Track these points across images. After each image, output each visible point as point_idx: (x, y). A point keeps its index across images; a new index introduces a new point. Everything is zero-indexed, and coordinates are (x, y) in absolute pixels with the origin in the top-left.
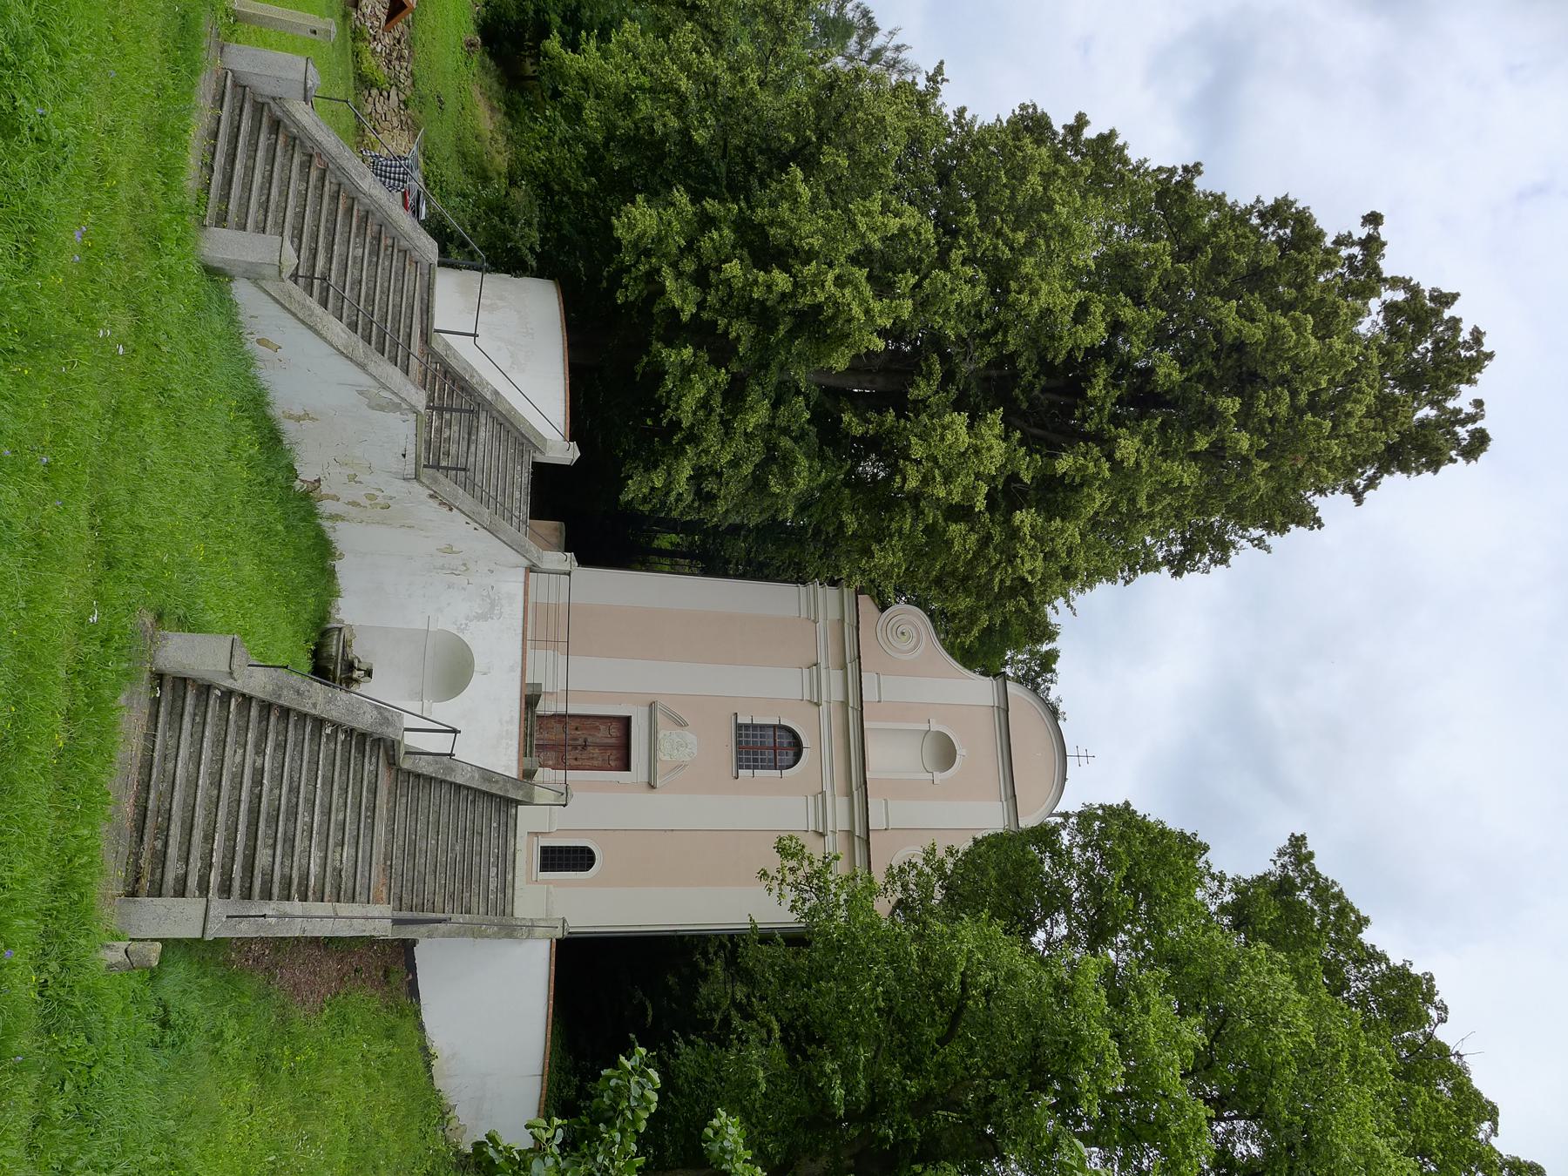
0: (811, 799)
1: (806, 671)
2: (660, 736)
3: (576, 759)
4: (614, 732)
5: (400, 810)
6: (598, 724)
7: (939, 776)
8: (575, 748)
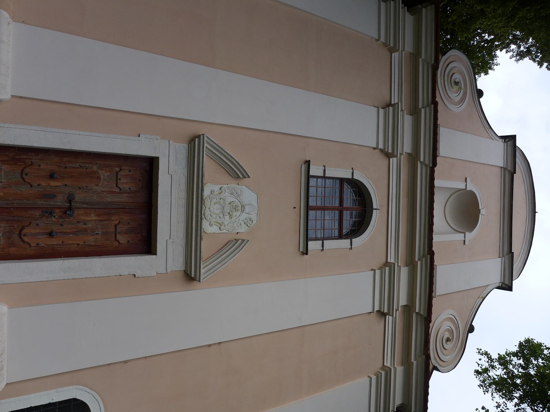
0: (378, 272)
1: (382, 111)
2: (206, 193)
3: (51, 234)
4: (126, 184)
5: (403, 11)
6: (95, 168)
7: (470, 236)
8: (49, 212)
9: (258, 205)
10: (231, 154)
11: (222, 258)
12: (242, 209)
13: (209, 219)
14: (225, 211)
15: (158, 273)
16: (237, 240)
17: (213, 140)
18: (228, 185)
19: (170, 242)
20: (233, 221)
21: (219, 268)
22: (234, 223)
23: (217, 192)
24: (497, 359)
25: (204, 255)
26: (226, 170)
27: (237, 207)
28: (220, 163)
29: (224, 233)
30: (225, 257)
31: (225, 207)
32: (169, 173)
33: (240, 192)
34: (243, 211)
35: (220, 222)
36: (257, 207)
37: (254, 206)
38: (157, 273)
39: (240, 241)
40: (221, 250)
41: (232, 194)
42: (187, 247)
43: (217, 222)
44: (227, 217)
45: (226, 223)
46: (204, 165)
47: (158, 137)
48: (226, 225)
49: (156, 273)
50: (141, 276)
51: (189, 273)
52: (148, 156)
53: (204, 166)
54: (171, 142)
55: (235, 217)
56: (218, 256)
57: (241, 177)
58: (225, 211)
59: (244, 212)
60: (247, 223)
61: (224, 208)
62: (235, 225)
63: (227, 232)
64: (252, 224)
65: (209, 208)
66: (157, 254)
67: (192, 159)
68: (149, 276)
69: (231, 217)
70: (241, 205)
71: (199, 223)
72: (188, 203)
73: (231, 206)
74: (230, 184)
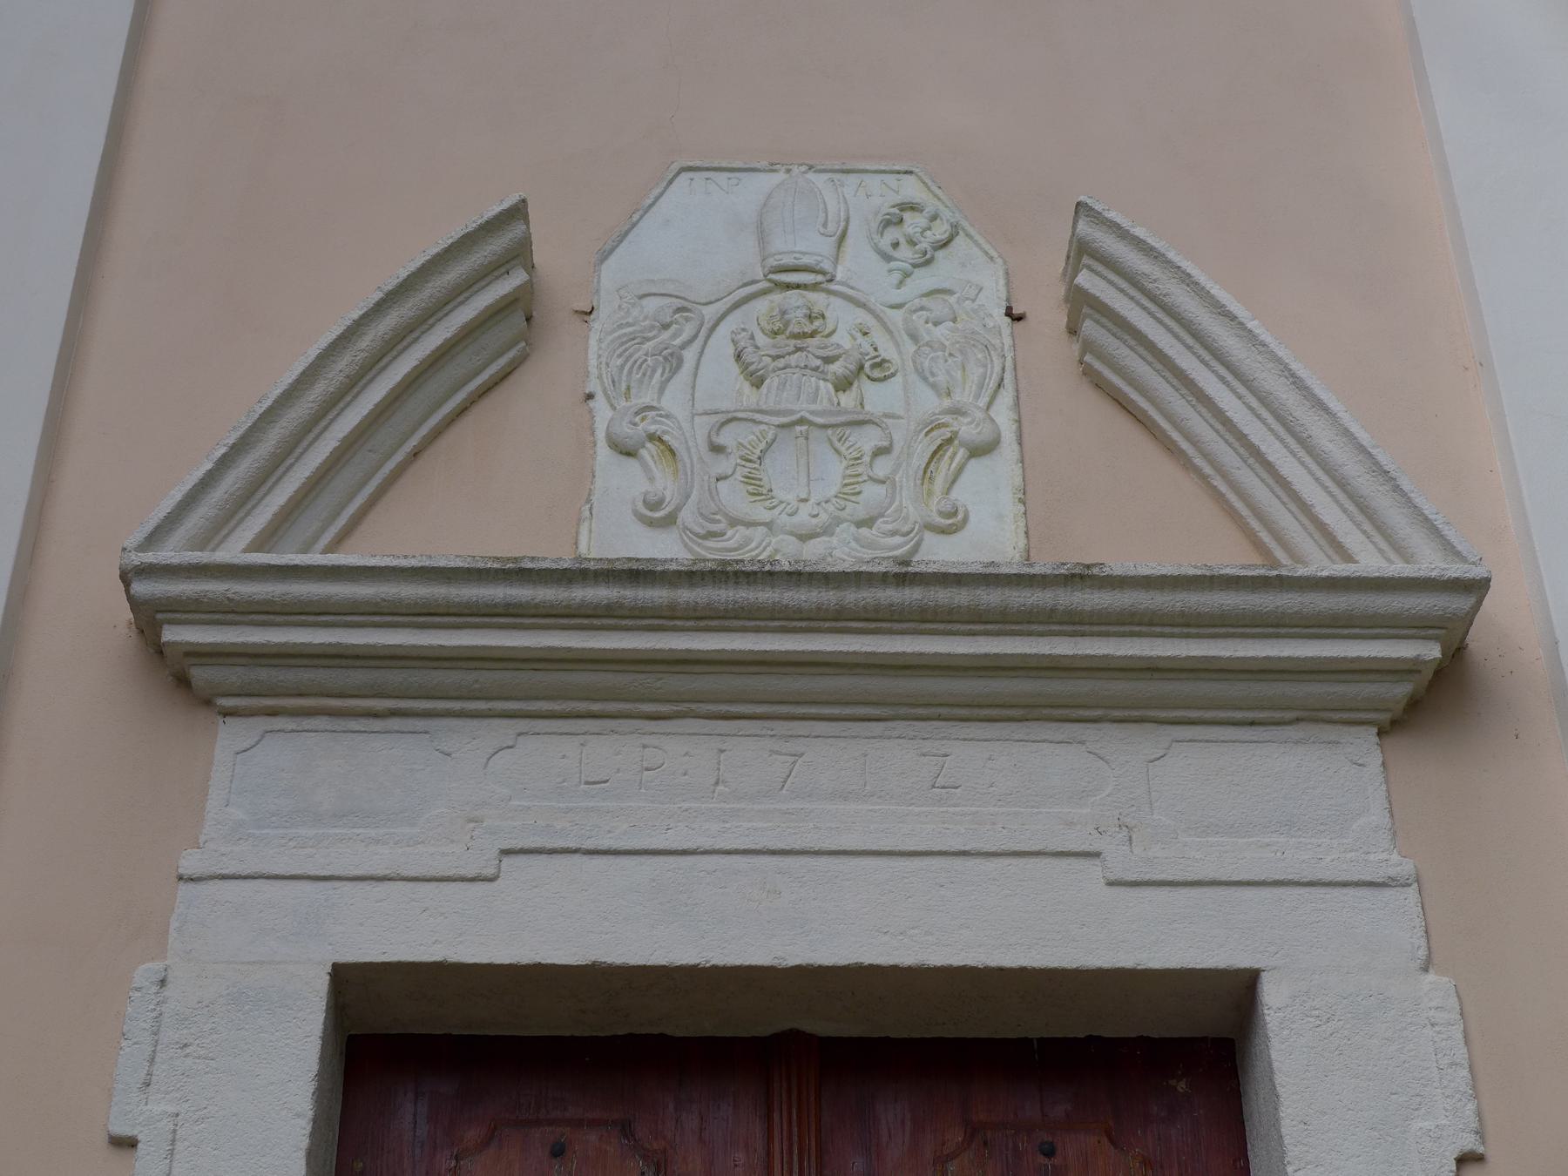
9: (764, 164)
10: (313, 353)
11: (1250, 416)
12: (798, 286)
13: (898, 540)
14: (831, 413)
15: (1422, 953)
16: (1080, 304)
17: (177, 495)
18: (590, 396)
19: (1121, 861)
20: (914, 348)
21: (1347, 433)
22: (927, 344)
23: (657, 473)
24: (1265, 563)
25: (1233, 558)
26: (462, 411)
27: (787, 324)
28: (399, 457)
29: (1019, 421)
30: (1242, 390)
31: (792, 412)
32: (489, 872)
33: (651, 304)
34: (821, 279)
35: (923, 448)
36: (779, 177)
37: (769, 196)
38: (1426, 970)
39: (1084, 279)
40: (1175, 435)
41: (673, 361)
42: (1163, 714)
43: (927, 474)
44: (877, 397)
45: (929, 403)
46: (404, 563)
47: (145, 973)
48: (947, 403)
49: (1431, 977)
50: (1471, 1106)
51: (1401, 690)
52: (322, 1059)
53: (414, 563)
54: (190, 863)
55: (879, 336)
56: (1228, 456)
57: (517, 278)
58: (831, 413)
59: (827, 266)
60: (924, 245)
61: (801, 421)
62: (940, 332)
63: (1006, 398)
64: (929, 210)
65: (804, 538)
66: (1243, 961)
67: (357, 677)
68: (1460, 1036)
69: (880, 369)
70: (764, 292)
71: (942, 596)
72: (760, 709)
73: (781, 363)
74: (587, 374)
